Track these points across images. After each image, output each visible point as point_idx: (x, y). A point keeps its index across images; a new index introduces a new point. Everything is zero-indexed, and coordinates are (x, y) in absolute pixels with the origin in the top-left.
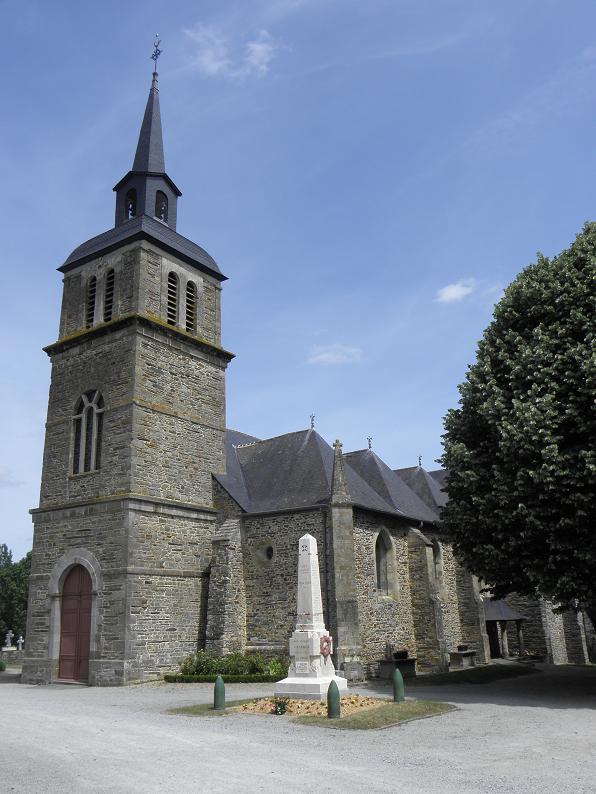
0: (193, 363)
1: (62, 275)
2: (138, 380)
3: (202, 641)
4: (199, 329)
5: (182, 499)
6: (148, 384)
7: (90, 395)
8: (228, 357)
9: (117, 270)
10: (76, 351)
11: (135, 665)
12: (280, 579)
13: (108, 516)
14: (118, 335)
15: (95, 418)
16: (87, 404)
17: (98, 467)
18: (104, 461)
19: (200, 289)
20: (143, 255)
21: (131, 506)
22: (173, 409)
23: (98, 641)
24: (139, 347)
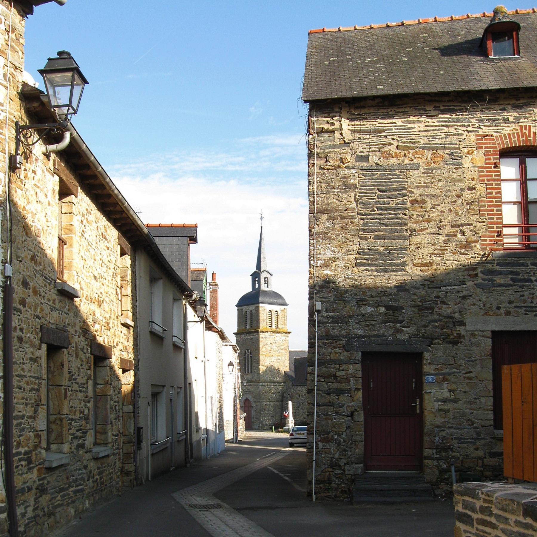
0: (278, 338)
1: (237, 308)
2: (260, 349)
3: (281, 419)
4: (279, 326)
5: (275, 380)
6: (264, 349)
7: (248, 350)
8: (290, 333)
9: (253, 312)
10: (243, 336)
11: (263, 425)
12: (301, 403)
13: (255, 387)
14: (255, 334)
15: (250, 358)
16: (247, 353)
17: (251, 372)
18: (253, 371)
19: (279, 312)
20: (260, 309)
21: (261, 384)
22: (271, 354)
23: (254, 418)
24: (261, 339)
